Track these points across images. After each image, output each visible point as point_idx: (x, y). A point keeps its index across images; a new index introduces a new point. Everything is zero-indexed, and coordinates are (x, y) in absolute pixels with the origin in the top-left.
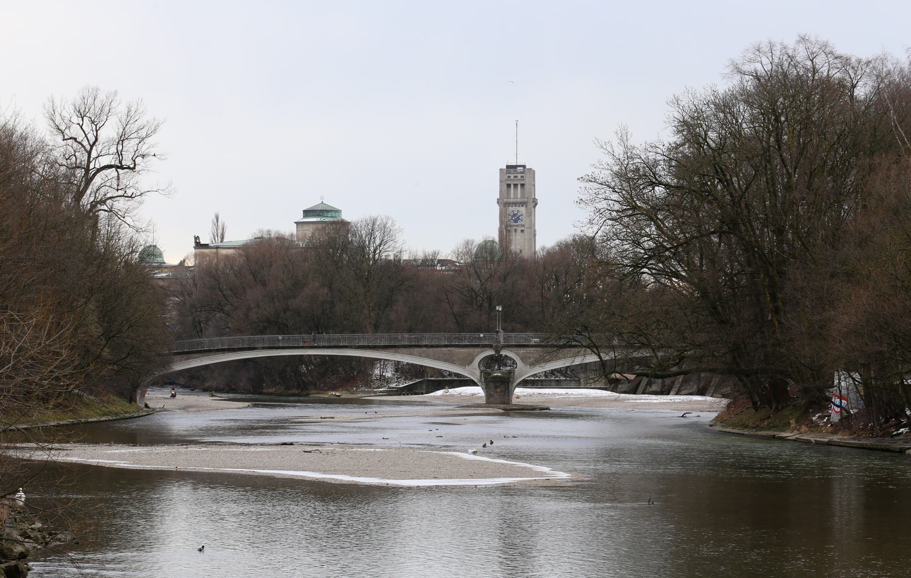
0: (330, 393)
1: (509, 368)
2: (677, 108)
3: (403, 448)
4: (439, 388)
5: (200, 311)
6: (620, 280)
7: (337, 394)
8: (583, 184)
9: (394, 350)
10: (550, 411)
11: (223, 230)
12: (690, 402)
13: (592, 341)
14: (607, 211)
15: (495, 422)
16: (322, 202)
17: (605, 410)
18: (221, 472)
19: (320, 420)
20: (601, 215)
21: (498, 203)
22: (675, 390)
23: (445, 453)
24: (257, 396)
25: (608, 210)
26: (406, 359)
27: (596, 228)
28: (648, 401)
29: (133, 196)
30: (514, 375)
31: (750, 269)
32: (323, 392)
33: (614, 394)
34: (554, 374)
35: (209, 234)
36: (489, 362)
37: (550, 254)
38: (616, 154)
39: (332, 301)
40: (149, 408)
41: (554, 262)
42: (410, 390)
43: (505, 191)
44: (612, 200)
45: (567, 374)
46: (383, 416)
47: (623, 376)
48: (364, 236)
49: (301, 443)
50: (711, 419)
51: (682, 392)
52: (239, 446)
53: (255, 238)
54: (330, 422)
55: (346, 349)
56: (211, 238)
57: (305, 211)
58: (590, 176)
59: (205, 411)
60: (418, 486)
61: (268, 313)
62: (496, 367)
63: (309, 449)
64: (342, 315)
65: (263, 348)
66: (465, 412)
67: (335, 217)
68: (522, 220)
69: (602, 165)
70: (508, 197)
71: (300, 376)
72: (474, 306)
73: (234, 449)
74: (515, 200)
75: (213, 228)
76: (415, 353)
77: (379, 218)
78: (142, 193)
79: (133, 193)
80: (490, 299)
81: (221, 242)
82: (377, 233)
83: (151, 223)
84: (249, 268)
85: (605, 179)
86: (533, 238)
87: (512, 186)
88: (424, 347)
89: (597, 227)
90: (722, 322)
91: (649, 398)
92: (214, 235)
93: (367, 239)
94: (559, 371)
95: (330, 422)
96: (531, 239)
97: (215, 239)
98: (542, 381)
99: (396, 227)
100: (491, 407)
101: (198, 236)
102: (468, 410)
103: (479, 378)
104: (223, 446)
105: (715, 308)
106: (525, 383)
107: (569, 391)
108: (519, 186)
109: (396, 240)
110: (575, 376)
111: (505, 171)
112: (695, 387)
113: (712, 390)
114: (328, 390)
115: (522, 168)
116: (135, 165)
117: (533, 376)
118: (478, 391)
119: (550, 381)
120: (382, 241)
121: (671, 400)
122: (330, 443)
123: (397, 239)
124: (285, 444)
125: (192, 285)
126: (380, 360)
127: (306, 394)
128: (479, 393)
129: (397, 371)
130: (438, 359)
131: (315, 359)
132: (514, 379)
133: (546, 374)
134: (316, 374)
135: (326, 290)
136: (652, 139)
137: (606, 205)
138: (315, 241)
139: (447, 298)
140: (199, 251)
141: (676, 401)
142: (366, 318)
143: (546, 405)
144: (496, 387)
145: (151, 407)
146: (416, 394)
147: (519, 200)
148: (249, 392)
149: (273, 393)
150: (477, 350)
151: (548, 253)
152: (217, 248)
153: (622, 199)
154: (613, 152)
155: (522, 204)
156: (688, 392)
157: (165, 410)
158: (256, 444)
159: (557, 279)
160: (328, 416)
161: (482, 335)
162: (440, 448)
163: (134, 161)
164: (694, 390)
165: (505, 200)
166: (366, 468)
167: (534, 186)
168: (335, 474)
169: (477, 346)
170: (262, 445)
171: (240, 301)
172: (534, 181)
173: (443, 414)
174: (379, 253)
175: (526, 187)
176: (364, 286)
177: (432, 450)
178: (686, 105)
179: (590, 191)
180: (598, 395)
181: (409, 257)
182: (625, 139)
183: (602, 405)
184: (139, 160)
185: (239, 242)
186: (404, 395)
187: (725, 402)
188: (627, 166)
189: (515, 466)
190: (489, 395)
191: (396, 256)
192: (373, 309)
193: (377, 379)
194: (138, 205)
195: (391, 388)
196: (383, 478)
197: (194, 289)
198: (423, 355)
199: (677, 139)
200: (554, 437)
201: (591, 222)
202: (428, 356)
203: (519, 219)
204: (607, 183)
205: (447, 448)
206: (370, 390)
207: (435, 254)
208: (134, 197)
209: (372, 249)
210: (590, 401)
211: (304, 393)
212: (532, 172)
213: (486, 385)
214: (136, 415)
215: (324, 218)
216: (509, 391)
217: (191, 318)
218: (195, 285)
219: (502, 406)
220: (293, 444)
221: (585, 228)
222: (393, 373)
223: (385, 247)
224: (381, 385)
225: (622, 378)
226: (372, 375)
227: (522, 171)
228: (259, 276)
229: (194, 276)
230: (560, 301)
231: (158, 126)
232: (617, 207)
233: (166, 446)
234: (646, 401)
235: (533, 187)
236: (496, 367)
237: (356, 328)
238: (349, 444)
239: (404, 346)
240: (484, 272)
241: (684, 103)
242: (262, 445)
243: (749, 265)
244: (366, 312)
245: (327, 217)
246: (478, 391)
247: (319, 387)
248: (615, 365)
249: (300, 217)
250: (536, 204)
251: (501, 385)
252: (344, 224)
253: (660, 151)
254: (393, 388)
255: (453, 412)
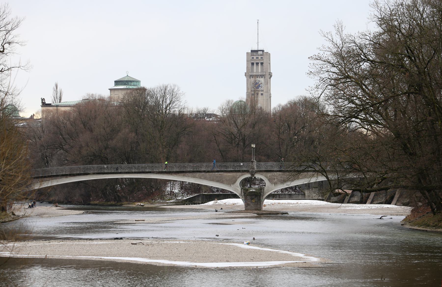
0: (137, 204)
1: (257, 186)
2: (377, 9)
3: (198, 241)
4: (210, 200)
5: (47, 149)
6: (337, 126)
7: (142, 204)
8: (312, 62)
9: (182, 174)
10: (288, 215)
11: (61, 94)
12: (382, 209)
13: (322, 168)
14: (328, 80)
15: (254, 222)
16: (127, 75)
17: (322, 214)
18: (79, 259)
19: (135, 222)
20: (324, 83)
21: (245, 75)
22: (369, 201)
23: (228, 244)
24: (86, 206)
25: (329, 79)
26: (189, 180)
27: (320, 91)
28: (354, 208)
29: (3, 70)
30: (264, 191)
31: (430, 118)
32: (132, 203)
33: (329, 203)
34: (287, 190)
35: (51, 97)
36: (244, 183)
37: (284, 109)
38: (335, 41)
39: (137, 142)
40: (15, 215)
41: (286, 115)
42: (191, 201)
43: (250, 68)
44: (331, 72)
45: (297, 190)
46: (177, 219)
47: (344, 191)
48: (159, 98)
49: (128, 238)
50: (401, 220)
51: (375, 202)
52: (85, 241)
53: (83, 100)
54: (142, 223)
55: (150, 174)
56: (52, 100)
57: (115, 82)
58: (317, 56)
59: (54, 217)
60: (218, 267)
61: (94, 150)
62: (248, 186)
63: (134, 242)
64: (145, 151)
65: (94, 174)
66: (231, 216)
67: (136, 85)
68: (262, 87)
69: (325, 48)
70: (252, 71)
71: (116, 192)
72: (234, 145)
73: (82, 242)
74: (257, 74)
75: (54, 93)
76: (197, 176)
77: (169, 86)
78: (9, 69)
79: (2, 69)
80: (244, 140)
81: (60, 102)
82: (168, 96)
83: (15, 89)
84: (80, 120)
85: (327, 58)
86: (269, 99)
87: (255, 64)
88: (203, 172)
89: (322, 90)
90: (411, 154)
91: (354, 206)
92: (54, 98)
93: (161, 100)
94: (291, 188)
95: (142, 223)
96: (268, 100)
97: (55, 100)
98: (279, 195)
99: (180, 92)
100: (249, 213)
101: (44, 99)
102: (234, 214)
103: (240, 193)
104: (74, 241)
105: (405, 145)
106: (272, 196)
107: (299, 201)
108: (260, 64)
109: (181, 101)
110: (302, 191)
111: (250, 55)
112: (384, 198)
113: (395, 201)
114: (136, 201)
115: (262, 52)
116: (4, 49)
117: (276, 191)
118: (240, 202)
119: (285, 194)
120: (171, 101)
121: (369, 207)
122: (147, 238)
123: (181, 100)
124: (117, 239)
125: (41, 131)
126: (170, 181)
127: (120, 205)
128: (238, 203)
129: (182, 188)
130: (213, 180)
131: (126, 181)
132: (263, 193)
133: (282, 190)
134: (127, 191)
135: (134, 134)
136: (363, 30)
137: (328, 76)
138: (125, 101)
139: (216, 140)
140: (45, 108)
141: (373, 208)
142: (161, 153)
143: (284, 211)
144: (252, 199)
145: (16, 214)
146: (194, 204)
147: (260, 73)
148: (80, 204)
149: (98, 204)
150: (240, 174)
151: (283, 109)
152: (57, 106)
153: (338, 71)
154: (333, 39)
155: (262, 76)
156: (379, 202)
157: (27, 217)
158: (97, 239)
159: (289, 126)
160: (139, 219)
161: (242, 164)
162: (223, 240)
163: (3, 46)
164: (383, 201)
165: (250, 73)
166: (178, 255)
167: (270, 64)
168: (158, 259)
169: (239, 171)
170: (101, 239)
171: (75, 142)
172: (270, 61)
173: (217, 217)
174: (169, 109)
175: (264, 65)
176: (159, 132)
177: (218, 242)
178: (383, 7)
179: (317, 66)
180: (318, 204)
181: (187, 112)
182: (341, 30)
183: (323, 211)
184: (6, 46)
185: (72, 102)
186: (187, 204)
187: (408, 210)
188: (342, 49)
189: (279, 253)
190: (247, 205)
191: (180, 111)
192: (165, 147)
193: (168, 194)
194: (6, 77)
195: (178, 200)
196: (192, 262)
197: (42, 134)
198: (202, 177)
199: (379, 30)
200: (295, 233)
201: (317, 87)
202: (205, 178)
203: (260, 86)
204: (328, 61)
205: (227, 240)
206: (164, 201)
207: (205, 110)
208: (3, 72)
209: (164, 106)
210: (314, 208)
211: (119, 204)
212: (268, 54)
213: (245, 198)
214: (7, 220)
215: (129, 86)
216: (260, 201)
217: (40, 154)
218: (43, 132)
219: (256, 212)
220: (122, 239)
221: (313, 92)
222: (179, 190)
223: (173, 105)
224: (171, 198)
225: (343, 192)
226: (165, 191)
227: (262, 54)
228: (88, 125)
229: (42, 125)
230: (291, 141)
231: (19, 22)
232: (335, 76)
233: (35, 241)
234: (352, 208)
235: (269, 65)
236: (248, 186)
237: (155, 160)
238: (160, 238)
239: (190, 172)
240: (240, 121)
241: (381, 5)
242: (101, 239)
243: (430, 116)
244: (161, 149)
245: (131, 85)
246: (240, 202)
247: (129, 200)
248: (339, 183)
249: (112, 86)
250: (271, 76)
251: (255, 197)
252: (144, 89)
253: (368, 38)
254: (179, 200)
255: (223, 216)
